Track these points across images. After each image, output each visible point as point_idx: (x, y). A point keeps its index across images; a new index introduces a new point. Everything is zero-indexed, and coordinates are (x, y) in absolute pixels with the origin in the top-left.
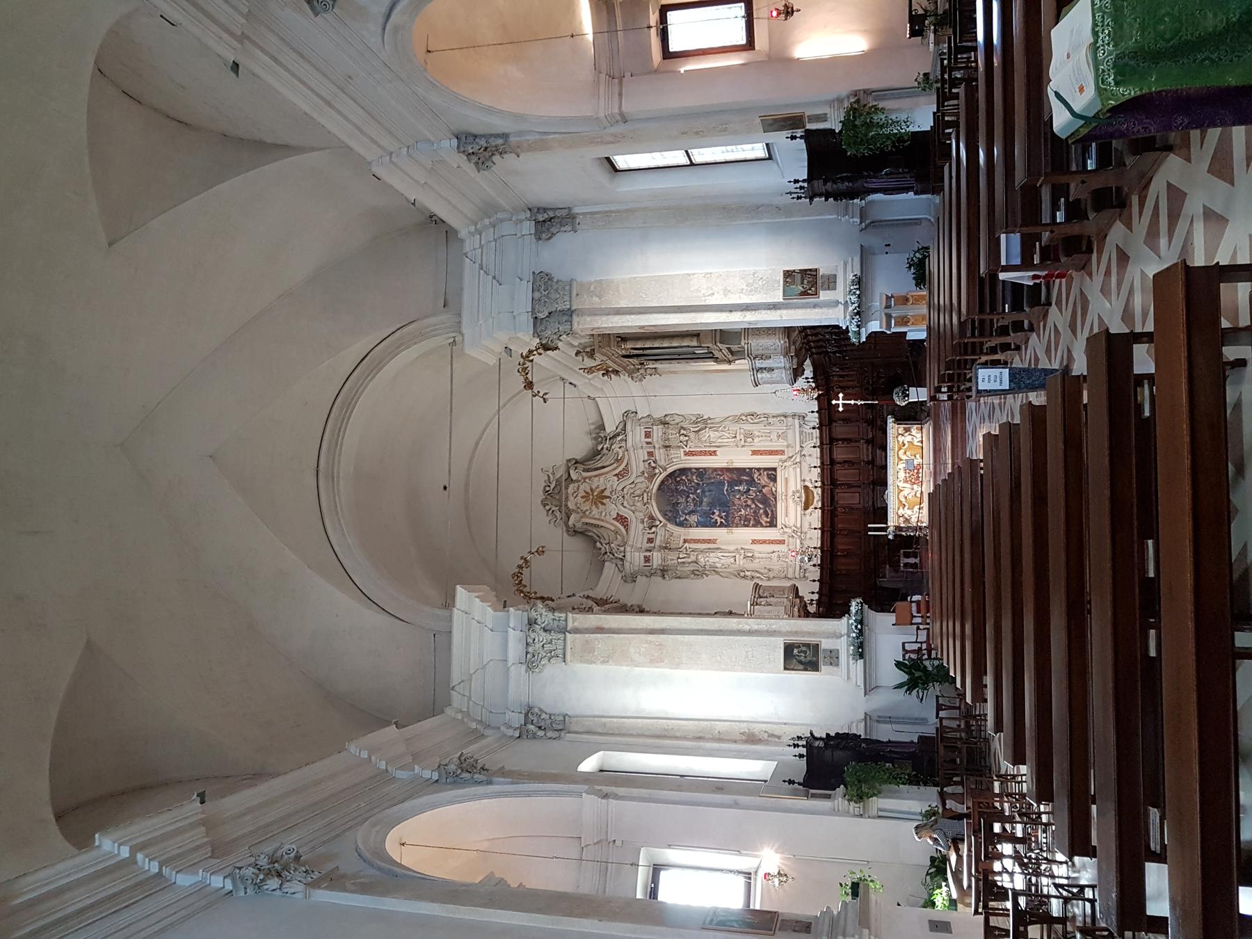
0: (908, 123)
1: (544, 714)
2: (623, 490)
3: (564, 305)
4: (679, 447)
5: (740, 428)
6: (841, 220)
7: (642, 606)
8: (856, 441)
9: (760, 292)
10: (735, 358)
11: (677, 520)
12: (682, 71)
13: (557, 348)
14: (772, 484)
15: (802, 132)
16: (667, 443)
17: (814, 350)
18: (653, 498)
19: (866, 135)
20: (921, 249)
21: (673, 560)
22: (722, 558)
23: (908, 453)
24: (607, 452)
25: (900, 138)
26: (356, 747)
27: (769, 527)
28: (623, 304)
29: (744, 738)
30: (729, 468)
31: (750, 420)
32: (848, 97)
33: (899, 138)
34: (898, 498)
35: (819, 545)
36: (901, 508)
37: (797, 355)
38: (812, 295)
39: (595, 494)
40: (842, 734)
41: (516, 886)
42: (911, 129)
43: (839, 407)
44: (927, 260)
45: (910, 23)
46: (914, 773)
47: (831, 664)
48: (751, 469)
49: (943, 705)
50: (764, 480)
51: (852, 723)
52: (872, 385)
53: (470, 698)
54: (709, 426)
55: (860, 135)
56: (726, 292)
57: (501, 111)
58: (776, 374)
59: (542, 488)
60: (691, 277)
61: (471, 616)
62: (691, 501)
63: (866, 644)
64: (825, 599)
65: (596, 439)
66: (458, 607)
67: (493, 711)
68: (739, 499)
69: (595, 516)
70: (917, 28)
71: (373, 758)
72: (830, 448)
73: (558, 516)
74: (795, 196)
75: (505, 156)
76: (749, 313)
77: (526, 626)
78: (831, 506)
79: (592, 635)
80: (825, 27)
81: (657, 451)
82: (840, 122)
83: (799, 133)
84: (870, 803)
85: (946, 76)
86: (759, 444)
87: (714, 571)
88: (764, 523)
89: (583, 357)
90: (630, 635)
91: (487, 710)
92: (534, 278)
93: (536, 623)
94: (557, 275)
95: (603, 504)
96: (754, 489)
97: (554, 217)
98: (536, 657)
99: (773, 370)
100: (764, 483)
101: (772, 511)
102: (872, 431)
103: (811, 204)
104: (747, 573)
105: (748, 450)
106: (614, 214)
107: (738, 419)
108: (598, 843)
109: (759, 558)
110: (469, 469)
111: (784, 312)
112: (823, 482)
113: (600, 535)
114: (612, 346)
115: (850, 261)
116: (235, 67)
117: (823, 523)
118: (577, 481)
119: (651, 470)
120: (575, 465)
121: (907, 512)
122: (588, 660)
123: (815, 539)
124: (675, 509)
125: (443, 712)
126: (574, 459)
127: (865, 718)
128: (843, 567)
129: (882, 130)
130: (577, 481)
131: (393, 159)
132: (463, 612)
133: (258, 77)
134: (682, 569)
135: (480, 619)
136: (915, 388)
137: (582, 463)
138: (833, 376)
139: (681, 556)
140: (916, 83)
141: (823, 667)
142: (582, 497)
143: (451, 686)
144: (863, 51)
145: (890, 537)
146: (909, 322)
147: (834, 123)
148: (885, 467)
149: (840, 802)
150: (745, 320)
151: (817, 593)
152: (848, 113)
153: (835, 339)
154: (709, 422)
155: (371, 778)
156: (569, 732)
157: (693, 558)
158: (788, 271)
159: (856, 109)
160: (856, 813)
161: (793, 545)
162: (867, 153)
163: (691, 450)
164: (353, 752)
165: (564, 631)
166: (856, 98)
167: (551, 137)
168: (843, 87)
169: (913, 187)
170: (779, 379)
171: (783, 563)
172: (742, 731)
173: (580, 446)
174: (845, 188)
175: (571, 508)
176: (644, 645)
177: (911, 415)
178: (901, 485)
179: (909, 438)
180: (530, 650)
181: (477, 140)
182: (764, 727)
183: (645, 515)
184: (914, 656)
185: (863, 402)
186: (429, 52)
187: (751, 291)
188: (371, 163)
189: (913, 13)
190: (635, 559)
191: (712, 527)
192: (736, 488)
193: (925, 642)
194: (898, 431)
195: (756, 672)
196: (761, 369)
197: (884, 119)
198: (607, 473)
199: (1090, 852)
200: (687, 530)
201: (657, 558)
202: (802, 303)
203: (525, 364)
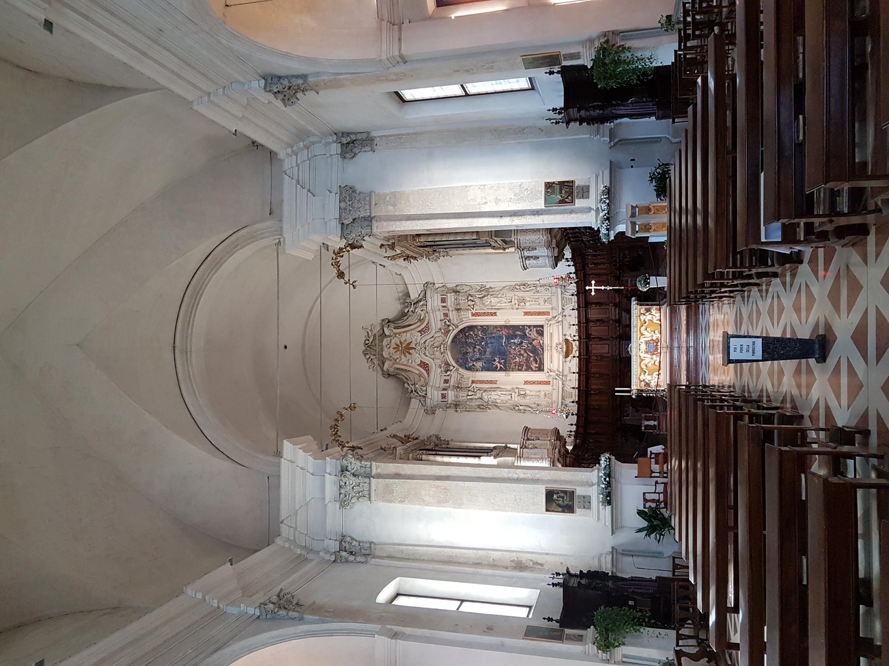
0: (652, 60)
1: (355, 541)
2: (425, 343)
3: (365, 213)
6: (593, 138)
9: (525, 201)
10: (507, 246)
11: (467, 365)
12: (453, 18)
13: (361, 247)
14: (540, 337)
15: (559, 68)
16: (458, 307)
18: (448, 349)
19: (614, 71)
20: (662, 166)
22: (501, 395)
23: (649, 329)
24: (412, 314)
25: (645, 74)
26: (193, 590)
28: (413, 211)
29: (514, 565)
30: (506, 326)
31: (522, 289)
32: (599, 38)
33: (644, 72)
34: (640, 366)
35: (577, 386)
36: (642, 374)
37: (557, 246)
39: (404, 346)
42: (654, 64)
44: (668, 180)
47: (584, 508)
48: (523, 326)
49: (678, 565)
50: (533, 334)
51: (602, 554)
52: (619, 263)
53: (296, 529)
54: (490, 293)
55: (609, 71)
56: (497, 201)
57: (298, 57)
59: (364, 342)
60: (469, 188)
61: (296, 464)
63: (613, 492)
64: (581, 430)
65: (404, 303)
66: (285, 456)
68: (515, 349)
71: (207, 598)
72: (585, 311)
74: (554, 121)
75: (306, 93)
76: (516, 218)
77: (339, 472)
78: (586, 355)
79: (391, 480)
81: (450, 312)
82: (591, 60)
84: (616, 652)
85: (689, 19)
86: (529, 307)
87: (495, 405)
88: (534, 368)
89: (386, 249)
90: (421, 481)
91: (310, 537)
92: (340, 191)
93: (347, 470)
94: (359, 188)
95: (410, 354)
97: (356, 139)
98: (347, 497)
99: (538, 258)
100: (533, 337)
101: (540, 359)
102: (619, 297)
105: (521, 312)
106: (404, 137)
107: (513, 288)
109: (530, 395)
110: (305, 331)
112: (580, 337)
113: (408, 377)
116: (48, 25)
118: (389, 336)
120: (389, 324)
121: (647, 378)
122: (389, 500)
123: (573, 380)
124: (465, 357)
125: (273, 542)
126: (387, 319)
130: (389, 336)
131: (211, 99)
132: (289, 461)
133: (73, 33)
134: (470, 404)
136: (655, 277)
138: (588, 255)
139: (469, 394)
140: (660, 24)
141: (577, 509)
142: (394, 348)
143: (281, 520)
146: (651, 229)
147: (586, 60)
148: (629, 326)
151: (575, 425)
152: (598, 52)
153: (588, 232)
154: (490, 290)
155: (202, 618)
156: (374, 558)
157: (478, 395)
158: (548, 183)
160: (604, 658)
162: (615, 86)
163: (477, 312)
164: (190, 594)
165: (369, 476)
166: (606, 39)
167: (342, 77)
168: (594, 29)
169: (655, 113)
170: (544, 264)
171: (548, 400)
172: (512, 559)
173: (392, 309)
175: (385, 356)
176: (432, 489)
177: (650, 298)
178: (643, 355)
179: (649, 317)
180: (342, 491)
181: (281, 81)
182: (530, 556)
183: (442, 362)
184: (653, 505)
186: (227, 6)
188: (192, 102)
190: (434, 395)
191: (493, 371)
192: (512, 341)
193: (662, 493)
195: (523, 512)
197: (630, 57)
198: (412, 330)
199: (763, 534)
200: (474, 373)
201: (451, 395)
203: (337, 259)
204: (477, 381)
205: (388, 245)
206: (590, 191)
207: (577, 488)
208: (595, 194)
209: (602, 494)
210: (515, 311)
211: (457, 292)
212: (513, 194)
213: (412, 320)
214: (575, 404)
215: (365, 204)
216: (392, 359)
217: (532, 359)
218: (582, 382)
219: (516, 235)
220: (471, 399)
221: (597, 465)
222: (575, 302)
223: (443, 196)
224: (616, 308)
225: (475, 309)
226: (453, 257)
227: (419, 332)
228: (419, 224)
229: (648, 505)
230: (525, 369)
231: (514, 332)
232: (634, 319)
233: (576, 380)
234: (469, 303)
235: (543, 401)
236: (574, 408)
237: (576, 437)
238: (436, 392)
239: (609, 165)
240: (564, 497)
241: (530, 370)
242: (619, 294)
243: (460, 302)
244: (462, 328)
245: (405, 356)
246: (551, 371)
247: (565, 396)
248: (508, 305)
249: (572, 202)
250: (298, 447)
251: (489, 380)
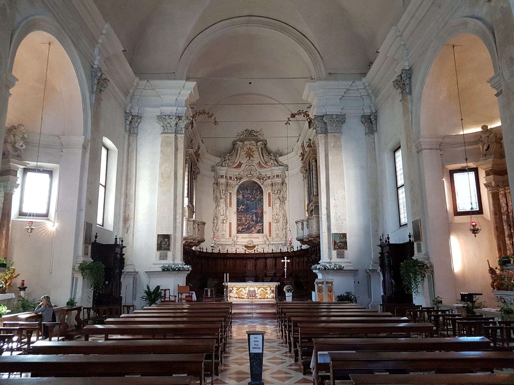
0: (416, 293)
2: (253, 165)
7: (199, 173)
8: (275, 269)
12: (443, 180)
13: (310, 127)
14: (256, 231)
15: (413, 240)
17: (313, 249)
19: (411, 272)
21: (222, 188)
24: (270, 158)
25: (409, 289)
27: (237, 230)
28: (330, 158)
29: (127, 216)
31: (284, 221)
32: (429, 263)
34: (241, 287)
35: (229, 252)
38: (335, 247)
39: (251, 153)
40: (124, 261)
41: (10, 92)
42: (414, 294)
43: (288, 262)
45: (469, 294)
46: (97, 295)
47: (160, 256)
48: (263, 222)
52: (299, 275)
53: (144, 89)
56: (336, 206)
57: (422, 89)
58: (301, 231)
61: (182, 89)
65: (276, 153)
67: (139, 101)
68: (249, 217)
70: (466, 298)
72: (272, 257)
74: (382, 238)
75: (401, 94)
76: (326, 217)
78: (246, 258)
79: (174, 146)
80: (466, 251)
81: (271, 180)
82: (417, 259)
83: (412, 239)
85: (440, 313)
86: (274, 225)
89: (308, 142)
94: (344, 126)
95: (247, 157)
98: (164, 120)
101: (244, 231)
102: (280, 275)
103: (378, 246)
105: (271, 221)
107: (284, 216)
108: (62, 144)
109: (223, 226)
110: (259, 95)
111: (326, 234)
112: (257, 254)
114: (314, 156)
115: (351, 265)
117: (238, 254)
118: (257, 145)
120: (264, 144)
121: (234, 291)
123: (232, 250)
127: (135, 272)
129: (413, 279)
130: (257, 145)
134: (218, 192)
135: (181, 94)
137: (265, 147)
138: (303, 258)
139: (224, 191)
140: (437, 297)
144: (454, 270)
145: (224, 284)
146: (320, 293)
147: (417, 256)
148: (263, 281)
149: (81, 259)
150: (323, 215)
151: (207, 251)
152: (422, 262)
154: (283, 203)
156: (129, 136)
157: (223, 196)
158: (346, 235)
159: (424, 266)
160: (75, 268)
165: (176, 133)
166: (429, 267)
168: (434, 260)
173: (272, 146)
174: (385, 262)
177: (280, 293)
178: (247, 289)
179: (269, 292)
180: (167, 117)
182: (132, 225)
184: (163, 295)
186: (453, 46)
187: (337, 218)
189: (474, 296)
190: (223, 171)
191: (237, 205)
192: (254, 216)
193: (170, 299)
194: (272, 287)
196: (303, 224)
197: (418, 280)
198: (260, 158)
201: (223, 181)
202: (330, 243)
206: (341, 259)
207: (172, 252)
209: (168, 266)
210: (272, 217)
213: (266, 158)
214: (219, 251)
217: (244, 227)
229: (163, 292)
234: (276, 191)
235: (220, 233)
236: (216, 251)
238: (224, 172)
239: (355, 269)
243: (277, 186)
245: (245, 154)
249: (335, 249)
251: (232, 202)
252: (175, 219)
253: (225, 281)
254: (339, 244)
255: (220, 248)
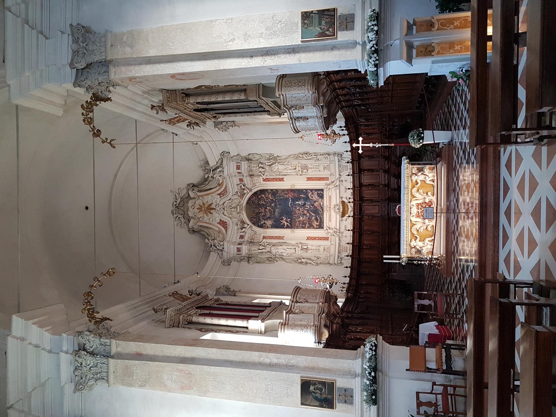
2: (223, 204)
4: (259, 175)
5: (299, 163)
13: (109, 99)
14: (320, 200)
21: (255, 250)
23: (421, 191)
24: (212, 179)
28: (152, 53)
31: (305, 157)
34: (411, 231)
35: (351, 242)
36: (413, 239)
39: (206, 206)
47: (346, 402)
48: (306, 190)
50: (315, 197)
52: (389, 132)
54: (278, 161)
56: (247, 37)
62: (268, 211)
64: (354, 283)
65: (205, 170)
68: (299, 210)
69: (206, 221)
73: (183, 221)
78: (360, 215)
79: (131, 362)
86: (312, 173)
94: (94, 28)
95: (211, 213)
96: (308, 203)
98: (84, 379)
99: (308, 119)
101: (320, 218)
104: (303, 260)
105: (304, 177)
107: (297, 157)
110: (111, 193)
112: (354, 199)
113: (209, 234)
117: (354, 227)
118: (194, 198)
119: (242, 191)
120: (193, 188)
121: (419, 244)
123: (348, 237)
128: (368, 257)
130: (194, 198)
134: (261, 256)
139: (260, 248)
141: (337, 404)
142: (198, 209)
145: (403, 264)
150: (266, 64)
151: (348, 277)
157: (268, 249)
158: (306, 13)
161: (334, 241)
165: (108, 356)
170: (313, 126)
171: (327, 253)
173: (196, 176)
178: (414, 219)
185: (380, 145)
190: (230, 249)
192: (297, 203)
194: (412, 170)
198: (213, 193)
201: (245, 249)
204: (268, 236)
205: (159, 106)
206: (355, 20)
207: (337, 379)
208: (361, 20)
209: (367, 391)
210: (299, 176)
211: (249, 160)
212: (264, 28)
213: (213, 184)
214: (349, 257)
215: (100, 46)
216: (196, 218)
217: (313, 218)
218: (355, 237)
219: (280, 90)
220: (262, 252)
221: (362, 347)
222: (350, 169)
223: (186, 34)
224: (385, 174)
225: (265, 175)
226: (240, 127)
227: (218, 194)
228: (160, 69)
229: (423, 409)
230: (308, 227)
231: (299, 195)
232: (404, 179)
233: (350, 236)
234: (260, 169)
235: (322, 255)
236: (348, 262)
237: (348, 291)
238: (232, 246)
240: (322, 389)
241: (312, 228)
242: (389, 161)
243: (253, 169)
244: (255, 191)
245: (207, 215)
246: (329, 229)
247: (341, 249)
248: (293, 172)
250: (30, 322)
251: (277, 236)
252: (270, 366)
253: (398, 261)
254: (323, 27)
255: (344, 254)
